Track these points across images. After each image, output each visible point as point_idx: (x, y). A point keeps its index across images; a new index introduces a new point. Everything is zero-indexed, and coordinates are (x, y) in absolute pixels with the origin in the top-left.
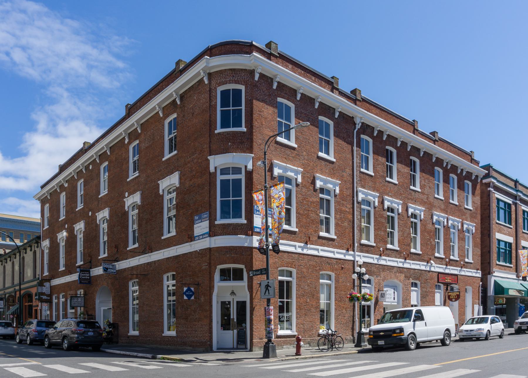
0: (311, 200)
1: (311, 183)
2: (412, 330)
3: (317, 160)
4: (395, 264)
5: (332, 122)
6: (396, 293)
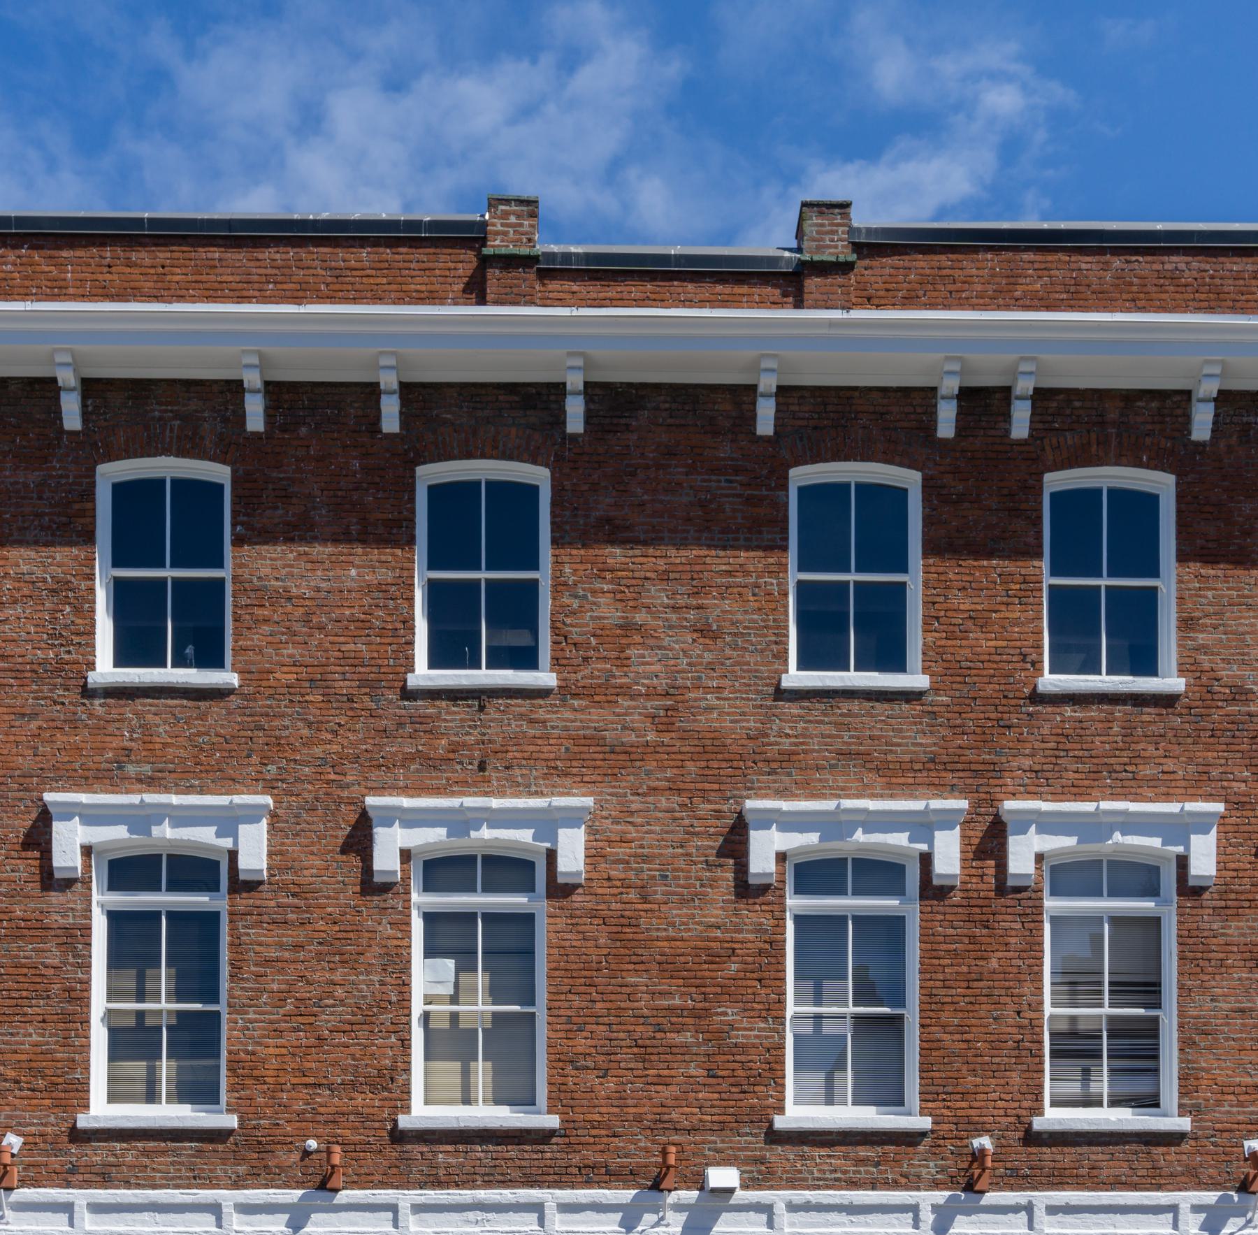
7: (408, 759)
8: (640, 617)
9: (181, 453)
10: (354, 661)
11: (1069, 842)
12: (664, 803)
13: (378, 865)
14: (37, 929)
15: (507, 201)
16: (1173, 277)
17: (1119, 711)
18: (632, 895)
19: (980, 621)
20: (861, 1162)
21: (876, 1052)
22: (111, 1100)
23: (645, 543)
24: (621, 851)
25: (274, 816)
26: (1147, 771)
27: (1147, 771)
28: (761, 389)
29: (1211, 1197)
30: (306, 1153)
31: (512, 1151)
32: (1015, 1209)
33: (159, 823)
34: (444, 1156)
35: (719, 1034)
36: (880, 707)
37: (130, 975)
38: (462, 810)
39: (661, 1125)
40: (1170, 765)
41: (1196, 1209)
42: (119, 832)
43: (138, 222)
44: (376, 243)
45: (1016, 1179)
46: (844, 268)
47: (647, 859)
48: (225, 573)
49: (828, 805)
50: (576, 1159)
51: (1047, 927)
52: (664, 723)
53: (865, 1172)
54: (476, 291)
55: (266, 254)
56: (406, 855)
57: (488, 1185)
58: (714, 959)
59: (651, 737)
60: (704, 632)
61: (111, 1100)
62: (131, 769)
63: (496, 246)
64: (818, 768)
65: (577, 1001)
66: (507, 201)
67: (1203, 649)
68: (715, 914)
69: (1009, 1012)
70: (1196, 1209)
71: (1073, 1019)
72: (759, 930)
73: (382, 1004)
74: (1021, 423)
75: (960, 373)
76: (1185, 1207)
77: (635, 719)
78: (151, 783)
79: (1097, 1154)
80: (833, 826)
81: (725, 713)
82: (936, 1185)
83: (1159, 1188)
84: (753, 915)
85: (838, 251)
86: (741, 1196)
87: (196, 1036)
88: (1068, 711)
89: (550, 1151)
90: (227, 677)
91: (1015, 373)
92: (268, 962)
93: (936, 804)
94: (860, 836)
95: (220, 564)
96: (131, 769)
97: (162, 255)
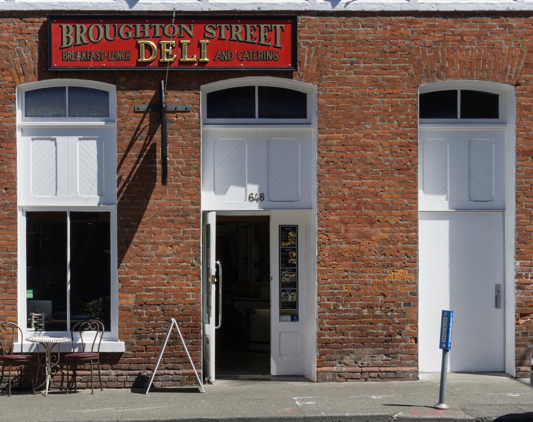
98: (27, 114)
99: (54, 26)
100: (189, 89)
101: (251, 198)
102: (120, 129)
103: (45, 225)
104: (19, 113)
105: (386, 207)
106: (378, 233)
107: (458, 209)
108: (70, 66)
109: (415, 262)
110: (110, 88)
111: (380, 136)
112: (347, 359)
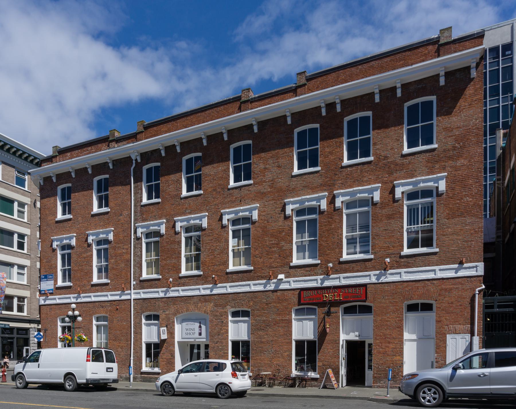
0: (85, 256)
1: (390, 193)
2: (21, 370)
3: (57, 225)
4: (197, 293)
5: (295, 130)
6: (203, 327)
7: (229, 201)
8: (267, 166)
9: (195, 152)
10: (220, 185)
11: (348, 198)
12: (271, 203)
13: (337, 205)
14: (174, 242)
15: (245, 90)
16: (372, 67)
17: (359, 167)
18: (266, 222)
19: (331, 153)
20: (307, 271)
21: (313, 248)
22: (234, 266)
23: (268, 151)
24: (264, 214)
25: (208, 216)
26: (365, 179)
27: (365, 179)
28: (472, 67)
29: (377, 272)
30: (213, 278)
31: (245, 274)
32: (337, 278)
33: (420, 183)
34: (234, 276)
35: (281, 248)
36: (311, 176)
37: (300, 235)
38: (237, 210)
39: (271, 267)
40: (370, 177)
41: (374, 275)
42: (185, 223)
43: (169, 118)
44: (224, 105)
45: (337, 272)
46: (304, 85)
47: (268, 214)
48: (319, 146)
49: (300, 198)
50: (256, 275)
51: (345, 217)
52: (271, 187)
53: (308, 273)
54: (240, 110)
55: (207, 112)
56: (228, 220)
57: (241, 281)
58: (280, 232)
59: (269, 190)
60: (279, 167)
61: (297, 259)
62: (187, 211)
63: (243, 99)
64: (299, 191)
65: (256, 244)
66: (245, 90)
67: (378, 149)
68: (280, 223)
69: (336, 236)
70: (374, 275)
71: (353, 235)
72: (288, 226)
73: (224, 249)
74: (339, 109)
75: (339, 98)
76: (372, 275)
77: (266, 187)
78: (190, 213)
79: (353, 265)
80: (302, 202)
81: (282, 182)
82: (321, 275)
83: (367, 271)
84: (287, 223)
85: (303, 81)
86: (285, 280)
87: (197, 258)
88: (349, 169)
89: (252, 274)
90: (371, 158)
91: (396, 83)
92: (207, 243)
93: (320, 194)
94: (307, 203)
95: (369, 134)
96: (187, 211)
97: (192, 117)
98: (232, 317)
99: (302, 292)
100: (337, 307)
101: (356, 336)
102: (319, 318)
103: (300, 344)
104: (293, 315)
105: (394, 338)
106: (391, 346)
107: (419, 339)
108: (305, 302)
109: (403, 354)
110: (316, 307)
111: (392, 318)
112: (381, 382)
